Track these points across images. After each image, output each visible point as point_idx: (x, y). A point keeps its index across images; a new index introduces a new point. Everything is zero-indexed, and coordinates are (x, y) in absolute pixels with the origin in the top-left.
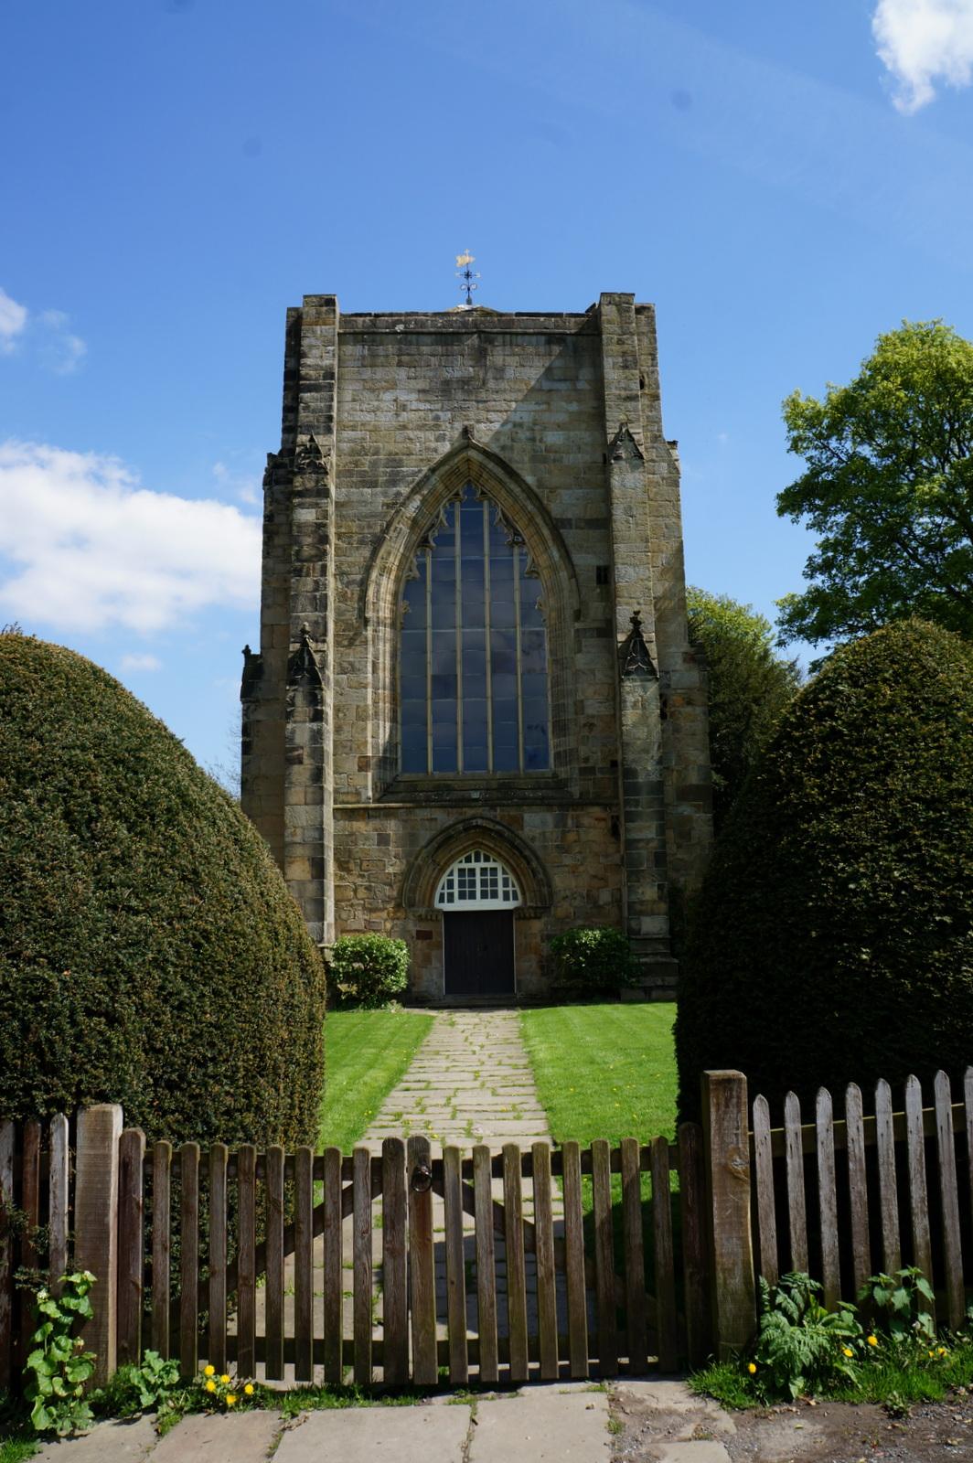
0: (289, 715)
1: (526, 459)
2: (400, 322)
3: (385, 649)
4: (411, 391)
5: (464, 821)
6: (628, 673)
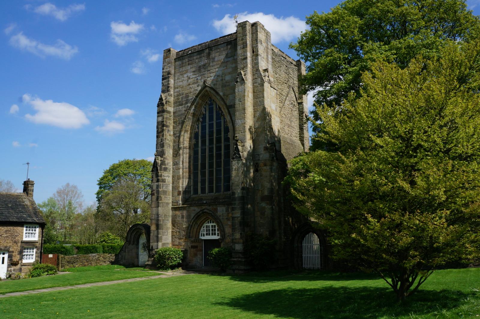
1: (220, 87)
5: (202, 210)
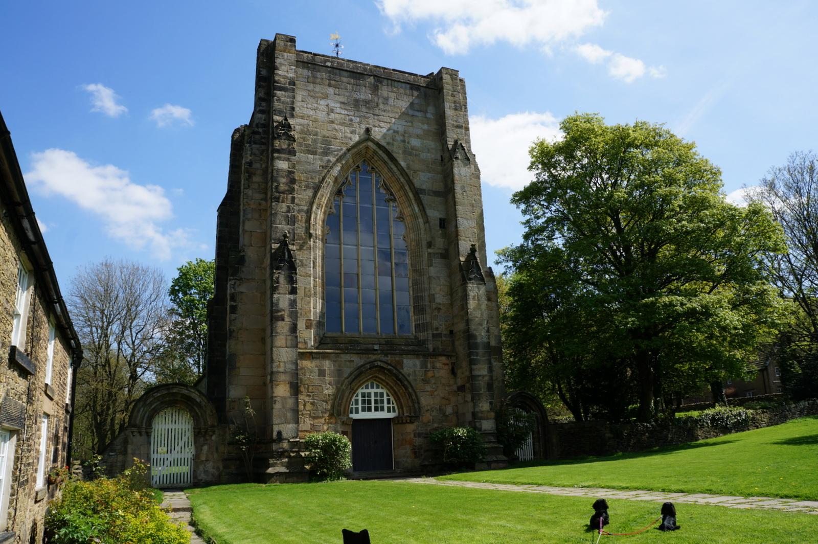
0: (274, 289)
1: (401, 152)
2: (329, 61)
3: (319, 253)
4: (336, 102)
6: (470, 279)
